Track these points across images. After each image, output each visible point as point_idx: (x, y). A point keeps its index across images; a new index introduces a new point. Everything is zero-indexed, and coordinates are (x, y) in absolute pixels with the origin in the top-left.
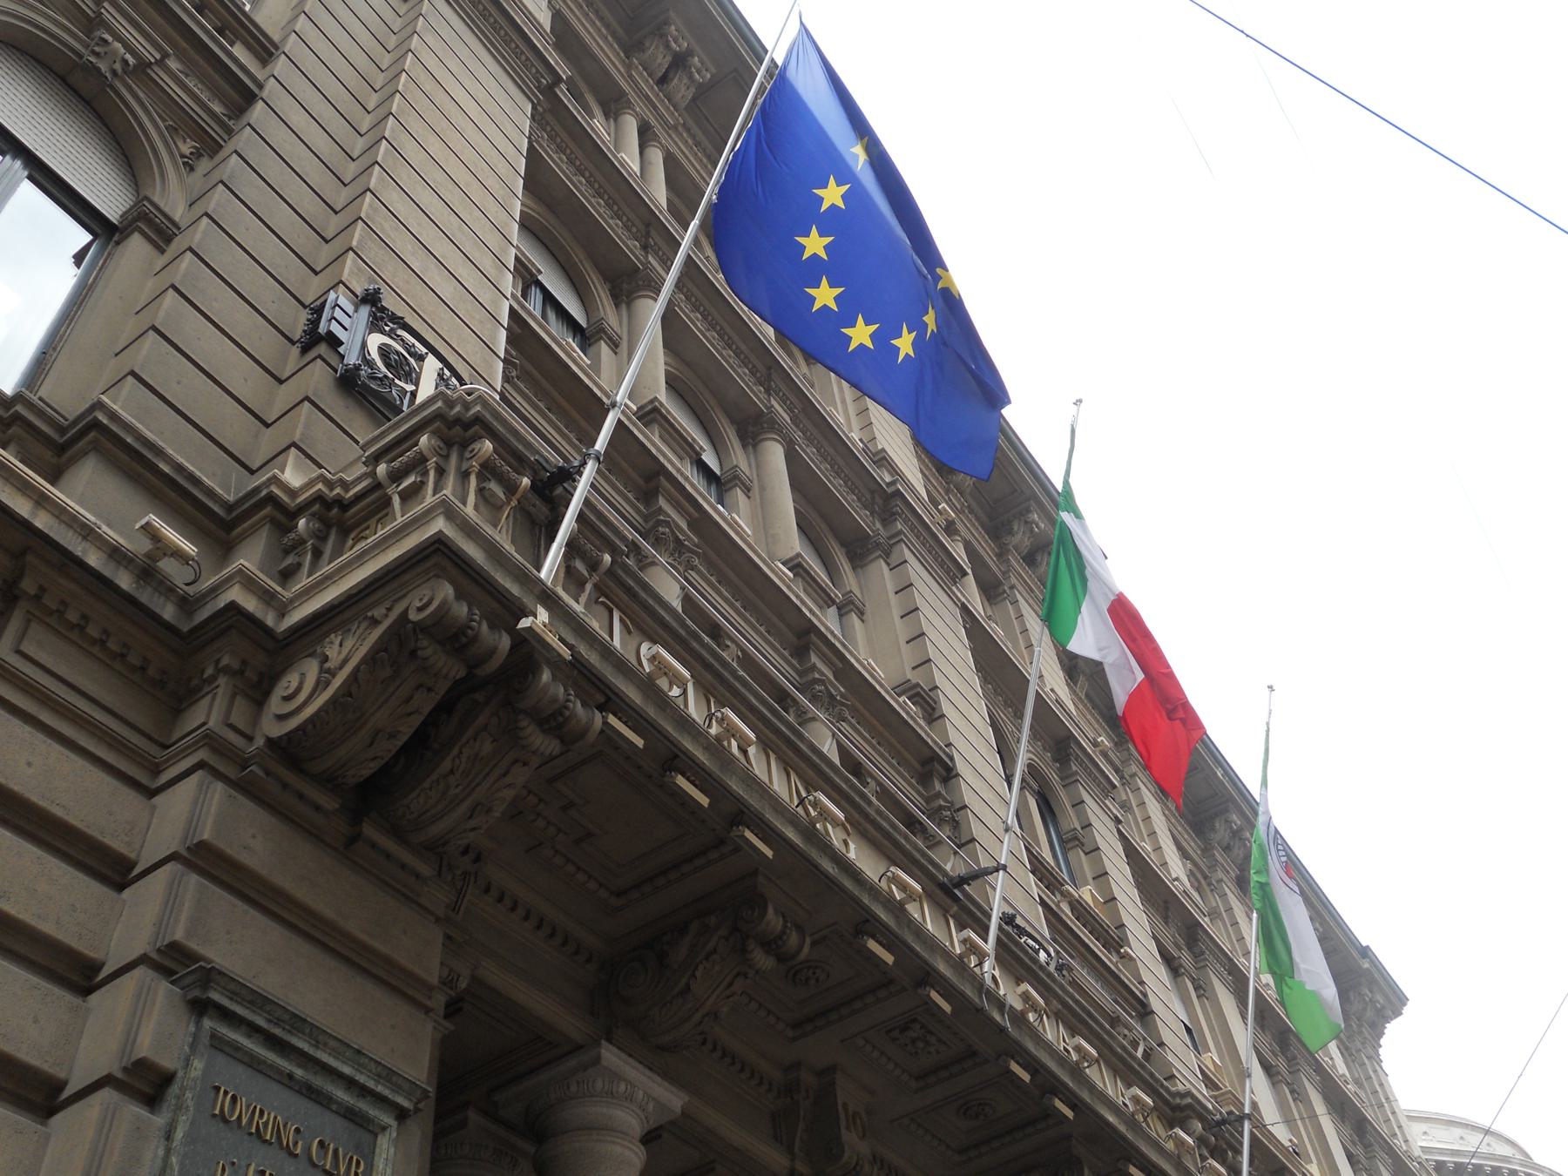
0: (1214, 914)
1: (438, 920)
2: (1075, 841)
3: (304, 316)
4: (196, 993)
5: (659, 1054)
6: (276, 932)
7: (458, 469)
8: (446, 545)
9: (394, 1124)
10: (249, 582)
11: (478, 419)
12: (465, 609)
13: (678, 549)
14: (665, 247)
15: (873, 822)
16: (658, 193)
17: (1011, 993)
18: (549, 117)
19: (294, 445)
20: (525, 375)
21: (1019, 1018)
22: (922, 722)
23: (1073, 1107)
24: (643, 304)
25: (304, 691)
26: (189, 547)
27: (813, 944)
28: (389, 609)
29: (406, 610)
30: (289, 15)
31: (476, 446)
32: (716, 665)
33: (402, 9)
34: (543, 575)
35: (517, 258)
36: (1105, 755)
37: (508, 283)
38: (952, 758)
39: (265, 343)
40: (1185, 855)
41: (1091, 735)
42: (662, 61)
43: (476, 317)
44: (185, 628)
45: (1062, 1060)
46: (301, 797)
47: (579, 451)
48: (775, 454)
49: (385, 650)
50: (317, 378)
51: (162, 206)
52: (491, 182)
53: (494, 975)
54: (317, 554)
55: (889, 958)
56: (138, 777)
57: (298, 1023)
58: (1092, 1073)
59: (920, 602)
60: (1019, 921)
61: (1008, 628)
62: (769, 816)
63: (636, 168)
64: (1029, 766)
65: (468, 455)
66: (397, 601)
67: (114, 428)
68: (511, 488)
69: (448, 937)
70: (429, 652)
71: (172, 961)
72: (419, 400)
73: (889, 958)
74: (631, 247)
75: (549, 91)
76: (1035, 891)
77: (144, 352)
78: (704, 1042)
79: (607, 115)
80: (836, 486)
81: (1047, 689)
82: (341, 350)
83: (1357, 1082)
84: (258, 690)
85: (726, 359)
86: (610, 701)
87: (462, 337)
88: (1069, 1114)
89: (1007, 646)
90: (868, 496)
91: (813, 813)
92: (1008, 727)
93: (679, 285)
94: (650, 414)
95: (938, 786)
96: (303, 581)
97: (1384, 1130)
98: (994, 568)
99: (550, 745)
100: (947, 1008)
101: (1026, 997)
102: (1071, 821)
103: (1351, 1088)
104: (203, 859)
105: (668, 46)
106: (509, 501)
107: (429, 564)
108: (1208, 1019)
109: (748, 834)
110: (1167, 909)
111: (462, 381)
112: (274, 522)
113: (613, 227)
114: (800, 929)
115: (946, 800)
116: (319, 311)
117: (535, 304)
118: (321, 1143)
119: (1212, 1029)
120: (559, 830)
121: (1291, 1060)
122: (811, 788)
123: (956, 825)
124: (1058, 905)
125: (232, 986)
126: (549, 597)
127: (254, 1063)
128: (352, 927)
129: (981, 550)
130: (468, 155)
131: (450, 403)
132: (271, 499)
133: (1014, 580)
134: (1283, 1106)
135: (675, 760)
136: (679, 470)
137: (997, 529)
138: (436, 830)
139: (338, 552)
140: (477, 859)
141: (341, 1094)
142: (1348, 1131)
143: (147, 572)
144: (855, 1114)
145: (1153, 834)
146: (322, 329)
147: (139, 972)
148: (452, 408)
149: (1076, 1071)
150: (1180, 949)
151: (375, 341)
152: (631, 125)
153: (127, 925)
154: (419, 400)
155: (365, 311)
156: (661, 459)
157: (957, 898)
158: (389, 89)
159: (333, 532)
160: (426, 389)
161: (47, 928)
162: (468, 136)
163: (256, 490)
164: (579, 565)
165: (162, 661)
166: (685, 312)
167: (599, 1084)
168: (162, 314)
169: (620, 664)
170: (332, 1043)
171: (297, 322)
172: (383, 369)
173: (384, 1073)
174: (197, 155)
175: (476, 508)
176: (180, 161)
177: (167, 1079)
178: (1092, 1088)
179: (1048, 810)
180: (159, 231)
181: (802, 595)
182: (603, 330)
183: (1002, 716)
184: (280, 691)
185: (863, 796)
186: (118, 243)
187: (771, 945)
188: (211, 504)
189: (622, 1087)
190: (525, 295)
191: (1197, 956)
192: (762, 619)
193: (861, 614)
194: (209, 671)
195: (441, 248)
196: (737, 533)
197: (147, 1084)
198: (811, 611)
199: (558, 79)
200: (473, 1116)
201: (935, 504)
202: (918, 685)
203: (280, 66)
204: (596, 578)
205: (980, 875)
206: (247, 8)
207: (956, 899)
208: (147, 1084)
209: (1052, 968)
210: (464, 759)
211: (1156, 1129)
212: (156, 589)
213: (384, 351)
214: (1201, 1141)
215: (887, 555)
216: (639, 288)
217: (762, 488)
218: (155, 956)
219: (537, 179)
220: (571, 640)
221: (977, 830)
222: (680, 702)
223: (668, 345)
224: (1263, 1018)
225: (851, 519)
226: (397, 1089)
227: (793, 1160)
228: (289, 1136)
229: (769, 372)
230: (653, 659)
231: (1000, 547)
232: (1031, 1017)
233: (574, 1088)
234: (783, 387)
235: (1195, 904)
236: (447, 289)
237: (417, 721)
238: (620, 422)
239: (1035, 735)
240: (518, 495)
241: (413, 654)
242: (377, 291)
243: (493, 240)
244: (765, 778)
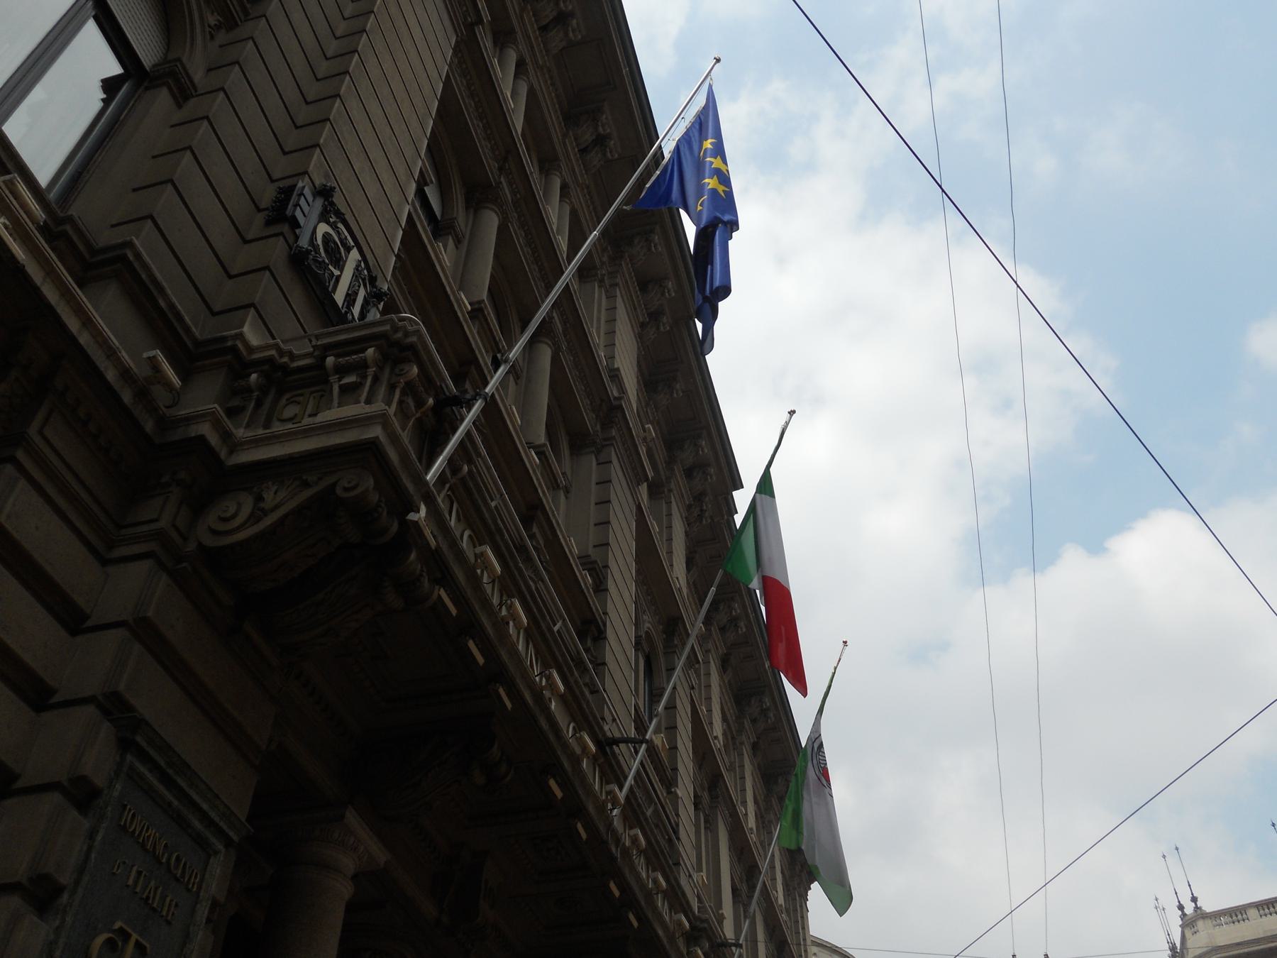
0: (731, 769)
11: (412, 347)
21: (626, 852)
23: (639, 920)
25: (237, 519)
28: (320, 479)
38: (605, 625)
40: (724, 719)
45: (643, 887)
50: (277, 251)
55: (559, 794)
59: (613, 497)
62: (519, 681)
67: (136, 265)
68: (420, 403)
71: (114, 706)
73: (559, 794)
75: (470, 27)
82: (297, 231)
83: (787, 911)
86: (444, 578)
88: (635, 924)
100: (584, 836)
103: (784, 917)
104: (143, 630)
113: (484, 148)
118: (178, 858)
132: (234, 349)
141: (197, 824)
143: (142, 394)
145: (709, 699)
149: (649, 896)
151: (323, 228)
152: (512, 57)
155: (319, 203)
162: (410, 59)
163: (224, 339)
165: (143, 464)
171: (268, 195)
172: (323, 254)
177: (95, 793)
186: (147, 89)
188: (185, 338)
195: (376, 154)
197: (83, 795)
208: (83, 795)
213: (326, 237)
219: (448, 112)
235: (722, 762)
236: (372, 190)
242: (333, 189)
243: (409, 151)
244: (523, 654)
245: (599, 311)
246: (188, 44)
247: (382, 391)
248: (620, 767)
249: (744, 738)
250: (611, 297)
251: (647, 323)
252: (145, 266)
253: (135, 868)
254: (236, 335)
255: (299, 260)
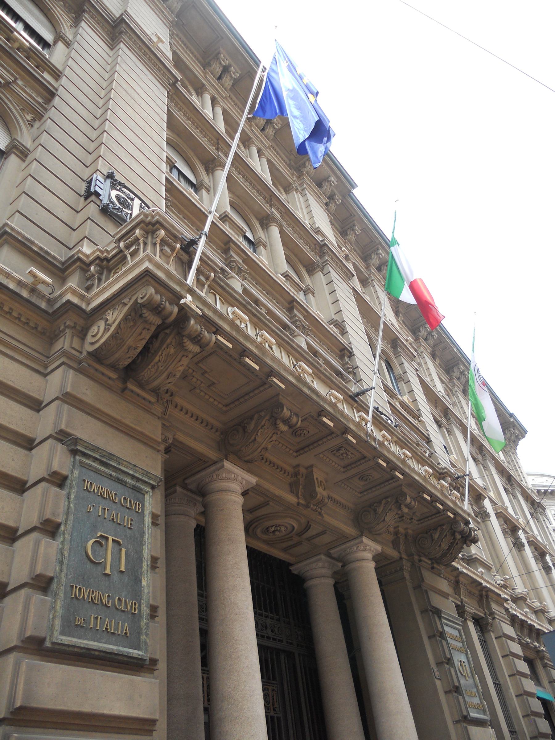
0: (454, 404)
1: (159, 418)
2: (400, 379)
3: (84, 185)
4: (73, 447)
5: (247, 463)
6: (99, 424)
7: (152, 242)
8: (150, 273)
9: (150, 490)
10: (74, 292)
11: (158, 222)
12: (159, 297)
13: (239, 271)
14: (225, 148)
15: (323, 373)
16: (221, 126)
17: (378, 435)
18: (175, 97)
19: (86, 237)
20: (174, 205)
22: (339, 335)
23: (402, 475)
24: (218, 173)
25: (100, 333)
26: (48, 280)
27: (302, 421)
28: (130, 299)
29: (137, 299)
30: (64, 59)
31: (158, 233)
32: (258, 315)
33: (111, 53)
34: (188, 282)
35: (166, 156)
36: (411, 345)
37: (164, 167)
38: (352, 349)
39: (70, 197)
40: (443, 382)
41: (405, 337)
42: (218, 70)
43: (153, 182)
44: (51, 311)
45: (398, 458)
46: (103, 374)
47: (197, 234)
48: (275, 231)
49: (130, 315)
50: (92, 210)
51: (22, 142)
52: (154, 125)
53: (181, 437)
54: (100, 280)
55: (331, 424)
56: (39, 369)
57: (111, 456)
58: (410, 462)
59: (336, 288)
60: (380, 409)
61: (371, 296)
62: (283, 372)
63: (211, 116)
64: (382, 350)
65: (155, 236)
66: (133, 295)
67: (13, 234)
68: (173, 249)
69: (163, 424)
70: (146, 315)
71: (62, 436)
72: (133, 216)
73: (331, 424)
74: (212, 149)
75: (174, 85)
76: (386, 399)
77: (21, 203)
78: (262, 459)
79: (198, 94)
80: (300, 243)
81: (388, 320)
82: (101, 198)
83: (508, 462)
84: (82, 334)
85: (253, 193)
86: (218, 330)
87: (149, 194)
88: (401, 477)
89: (371, 303)
90: (313, 246)
91: (299, 370)
92: (373, 336)
93: (232, 164)
94: (224, 218)
95: (347, 359)
96: (95, 290)
97: (518, 479)
98: (365, 273)
99: (196, 349)
100: (354, 441)
101: (384, 436)
102: (398, 371)
104: (67, 398)
105: (220, 63)
106: (173, 254)
107: (144, 280)
108: (452, 443)
109: (275, 380)
110: (436, 403)
111: (149, 208)
112: (82, 269)
113: (204, 141)
114: (297, 415)
115: (350, 365)
116: (90, 182)
117: (175, 176)
119: (454, 446)
120: (202, 382)
121: (483, 456)
122: (297, 361)
123: (354, 374)
124: (395, 403)
125: (85, 444)
126: (191, 291)
127: (97, 471)
128: (127, 422)
129: (359, 266)
130: (144, 115)
131: (146, 216)
132: (79, 259)
133: (373, 278)
134: (480, 472)
135: (244, 352)
136: (237, 240)
137: (366, 258)
138: (155, 384)
139: (107, 278)
140: (171, 395)
141: (129, 481)
142: (504, 480)
143: (33, 290)
144: (321, 482)
145: (430, 374)
146: (92, 190)
147: (50, 441)
148: (147, 218)
149: (403, 462)
150: (441, 418)
151: (114, 193)
152: (207, 98)
153: (44, 424)
154: (133, 216)
155: (109, 181)
156: (230, 236)
157: (356, 400)
158: (109, 88)
159: (105, 270)
160: (136, 211)
161: (12, 426)
164: (202, 278)
165: (46, 324)
166: (235, 175)
167: (224, 475)
168: (27, 187)
169: (221, 316)
170: (125, 463)
171: (82, 188)
173: (145, 473)
174: (34, 120)
175: (160, 257)
176: (27, 123)
177: (65, 478)
178: (409, 467)
179: (390, 367)
180: (22, 152)
181: (289, 287)
182: (203, 185)
183: (370, 331)
184: (90, 334)
185: (318, 363)
186: (5, 159)
187: (286, 421)
188: (55, 262)
189: (233, 475)
190: (171, 172)
191: (448, 420)
192: (274, 298)
193: (313, 294)
194: (62, 328)
195: (136, 154)
196: (262, 263)
197: (59, 480)
198: (293, 293)
199: (177, 80)
200: (178, 489)
201: (341, 248)
202: (337, 320)
203: (64, 81)
204: (209, 283)
205: (363, 393)
206: (47, 56)
207: (356, 401)
208: (59, 480)
209: (393, 425)
210: (164, 356)
211: (434, 481)
212: (37, 297)
213: (118, 197)
214: (450, 485)
215: (322, 270)
216: (216, 166)
217: (271, 245)
218: (55, 435)
220: (201, 307)
221: (363, 376)
222: (245, 329)
223: (229, 189)
224: (473, 441)
225: (308, 256)
226: (150, 478)
227: (298, 499)
228: (113, 496)
229: (271, 198)
230: (233, 313)
231: (367, 265)
232: (386, 443)
233: (215, 477)
234: (277, 203)
236: (140, 171)
237: (144, 342)
238: (213, 221)
239: (384, 338)
240: (176, 251)
241: (141, 316)
242: (113, 173)
243: (157, 149)
245: (300, 203)
246: (19, 131)
247: (149, 247)
248: (365, 404)
249: (456, 389)
250: (304, 195)
251: (328, 202)
252: (19, 233)
253: (100, 508)
254: (77, 251)
255: (105, 211)
